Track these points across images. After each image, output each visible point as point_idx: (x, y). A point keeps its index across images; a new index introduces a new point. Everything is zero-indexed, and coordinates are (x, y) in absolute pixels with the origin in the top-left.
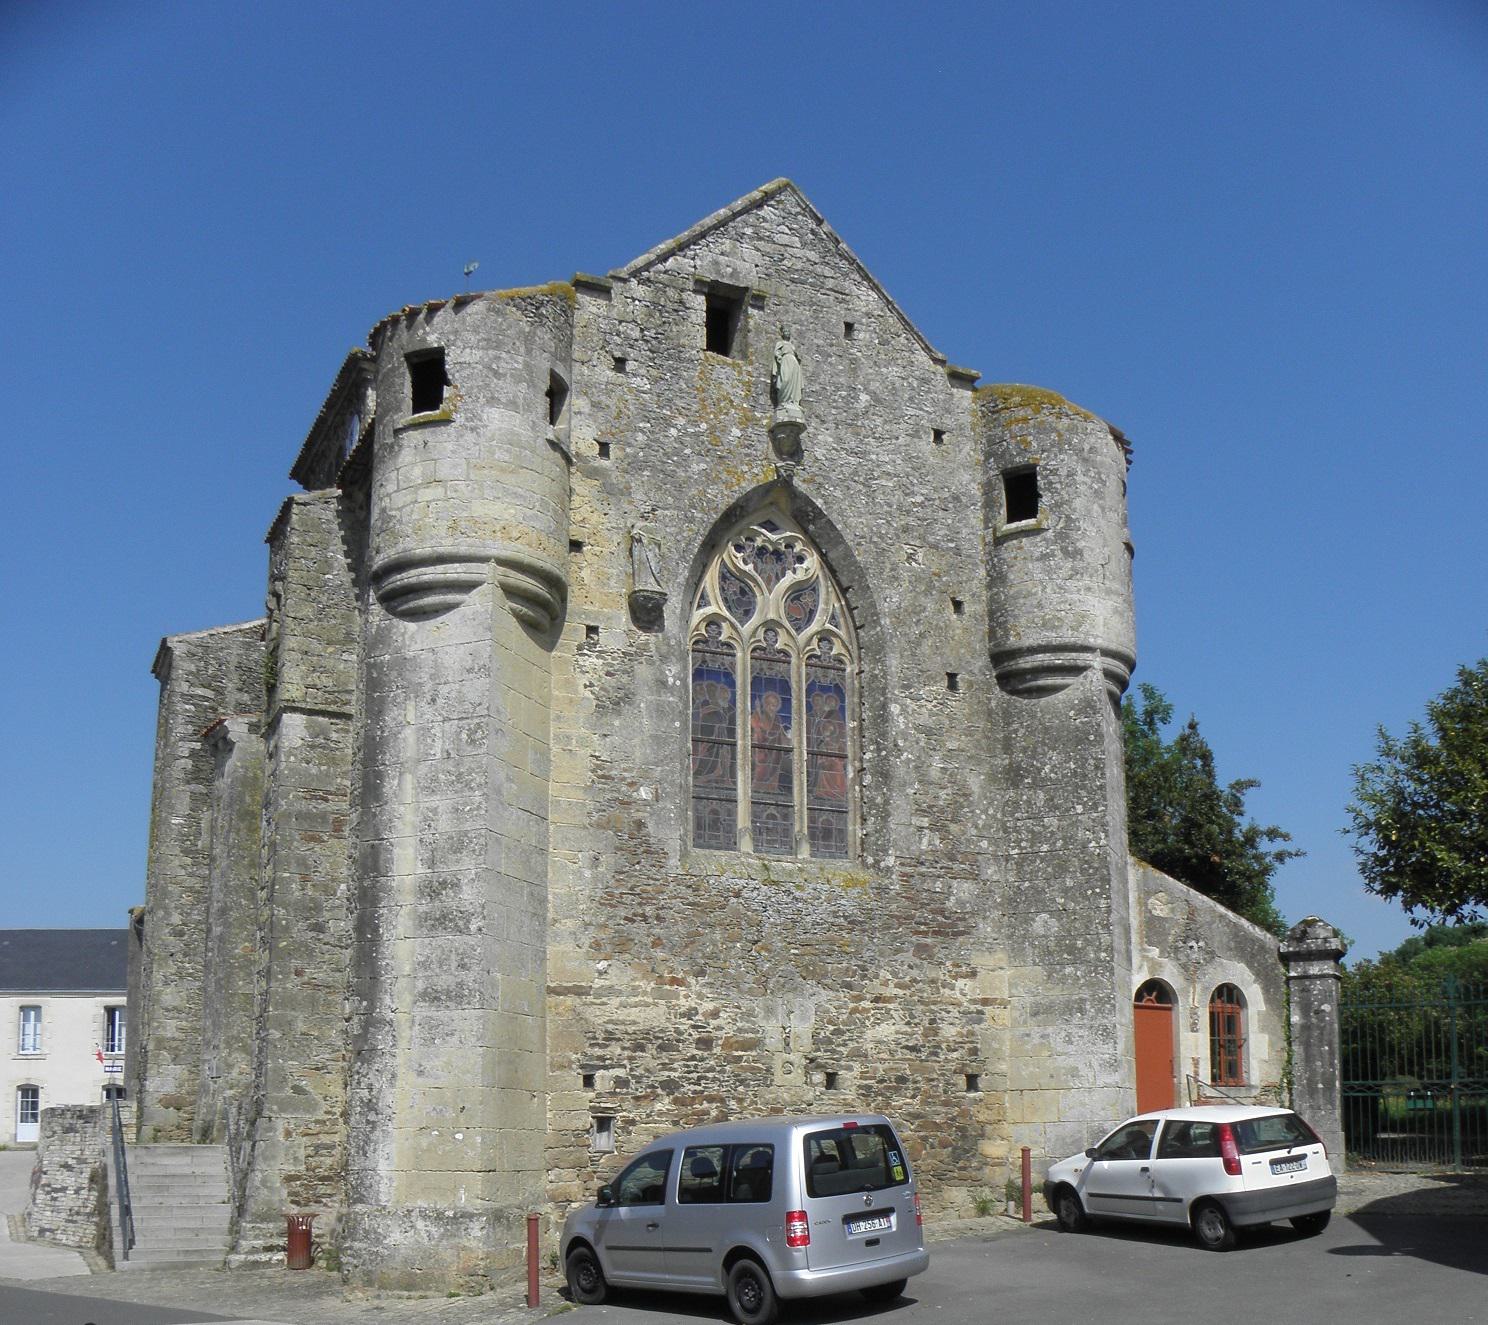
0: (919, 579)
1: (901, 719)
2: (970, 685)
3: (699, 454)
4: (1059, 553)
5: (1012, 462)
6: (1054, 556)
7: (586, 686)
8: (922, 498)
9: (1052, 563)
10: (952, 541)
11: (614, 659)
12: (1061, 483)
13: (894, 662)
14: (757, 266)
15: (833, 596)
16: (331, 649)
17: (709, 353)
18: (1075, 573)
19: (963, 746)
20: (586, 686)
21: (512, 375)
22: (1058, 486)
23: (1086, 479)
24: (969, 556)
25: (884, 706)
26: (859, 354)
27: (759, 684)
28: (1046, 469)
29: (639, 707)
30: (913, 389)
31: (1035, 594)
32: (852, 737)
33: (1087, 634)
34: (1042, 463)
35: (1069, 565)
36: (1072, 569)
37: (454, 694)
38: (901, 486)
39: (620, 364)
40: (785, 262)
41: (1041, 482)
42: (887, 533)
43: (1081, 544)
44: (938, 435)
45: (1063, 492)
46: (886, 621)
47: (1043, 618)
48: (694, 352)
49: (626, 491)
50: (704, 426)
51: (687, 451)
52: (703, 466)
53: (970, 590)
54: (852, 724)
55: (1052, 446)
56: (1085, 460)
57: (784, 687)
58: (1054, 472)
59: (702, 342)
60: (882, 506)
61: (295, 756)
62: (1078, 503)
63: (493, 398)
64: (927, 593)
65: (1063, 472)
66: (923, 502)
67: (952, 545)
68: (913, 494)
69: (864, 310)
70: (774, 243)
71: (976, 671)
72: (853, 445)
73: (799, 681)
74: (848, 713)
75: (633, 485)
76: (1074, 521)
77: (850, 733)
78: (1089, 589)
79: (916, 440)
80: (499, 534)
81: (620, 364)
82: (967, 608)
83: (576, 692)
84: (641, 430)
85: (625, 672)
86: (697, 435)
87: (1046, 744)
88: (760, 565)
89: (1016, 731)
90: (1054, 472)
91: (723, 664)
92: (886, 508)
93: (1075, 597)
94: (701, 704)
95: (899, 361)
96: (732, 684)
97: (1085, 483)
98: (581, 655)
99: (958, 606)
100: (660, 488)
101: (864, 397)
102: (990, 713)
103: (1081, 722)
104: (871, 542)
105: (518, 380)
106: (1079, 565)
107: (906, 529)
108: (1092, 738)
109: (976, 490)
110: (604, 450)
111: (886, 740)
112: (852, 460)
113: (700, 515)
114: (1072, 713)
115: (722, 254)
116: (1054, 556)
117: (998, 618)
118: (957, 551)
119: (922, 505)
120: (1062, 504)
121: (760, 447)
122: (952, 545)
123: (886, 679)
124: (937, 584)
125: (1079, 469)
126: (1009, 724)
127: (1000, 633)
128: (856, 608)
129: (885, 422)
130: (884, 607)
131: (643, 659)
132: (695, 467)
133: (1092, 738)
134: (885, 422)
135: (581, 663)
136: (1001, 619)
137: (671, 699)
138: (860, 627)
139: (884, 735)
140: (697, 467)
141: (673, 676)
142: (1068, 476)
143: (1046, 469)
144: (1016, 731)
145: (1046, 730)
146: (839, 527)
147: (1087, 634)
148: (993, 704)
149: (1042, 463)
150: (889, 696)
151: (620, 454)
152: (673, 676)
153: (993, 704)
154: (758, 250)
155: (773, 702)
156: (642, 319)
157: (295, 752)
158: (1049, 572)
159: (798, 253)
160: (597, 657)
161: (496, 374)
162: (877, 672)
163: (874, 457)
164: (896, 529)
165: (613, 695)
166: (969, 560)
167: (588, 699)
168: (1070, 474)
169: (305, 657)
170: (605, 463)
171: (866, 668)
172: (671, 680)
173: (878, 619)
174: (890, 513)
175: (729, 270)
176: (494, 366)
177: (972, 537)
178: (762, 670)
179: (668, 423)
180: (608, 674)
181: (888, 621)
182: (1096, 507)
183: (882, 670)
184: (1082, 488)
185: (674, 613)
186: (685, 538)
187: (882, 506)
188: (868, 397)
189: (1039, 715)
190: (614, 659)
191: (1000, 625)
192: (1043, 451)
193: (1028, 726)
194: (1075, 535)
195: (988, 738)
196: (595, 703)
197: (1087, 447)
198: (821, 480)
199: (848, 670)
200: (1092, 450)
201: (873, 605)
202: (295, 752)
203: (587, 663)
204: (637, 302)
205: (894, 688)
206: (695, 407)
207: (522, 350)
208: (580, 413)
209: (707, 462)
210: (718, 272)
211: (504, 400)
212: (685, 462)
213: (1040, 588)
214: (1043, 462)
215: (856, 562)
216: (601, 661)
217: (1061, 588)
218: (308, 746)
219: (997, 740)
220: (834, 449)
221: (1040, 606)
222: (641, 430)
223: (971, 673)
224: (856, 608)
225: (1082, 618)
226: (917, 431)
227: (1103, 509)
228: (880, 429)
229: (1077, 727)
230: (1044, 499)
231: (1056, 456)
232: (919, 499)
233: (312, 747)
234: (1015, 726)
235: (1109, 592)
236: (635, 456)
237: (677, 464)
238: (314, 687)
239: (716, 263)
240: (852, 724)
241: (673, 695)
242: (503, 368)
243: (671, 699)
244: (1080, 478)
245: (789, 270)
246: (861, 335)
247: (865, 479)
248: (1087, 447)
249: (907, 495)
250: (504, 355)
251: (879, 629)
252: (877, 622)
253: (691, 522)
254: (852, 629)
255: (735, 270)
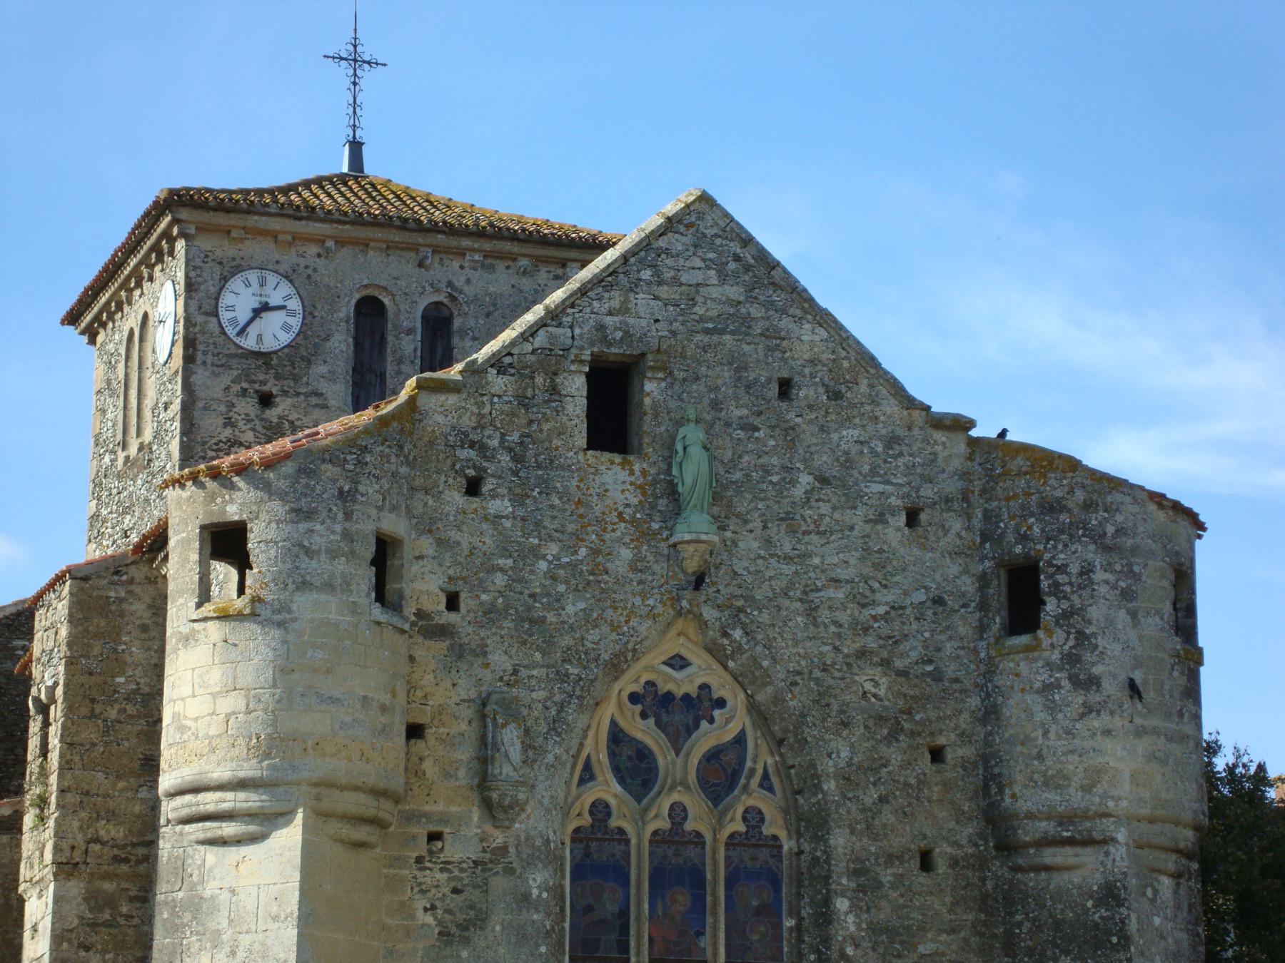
0: (880, 719)
1: (851, 918)
2: (954, 863)
3: (576, 590)
4: (1066, 683)
5: (1010, 552)
6: (1059, 687)
7: (426, 910)
8: (887, 608)
9: (1057, 697)
10: (930, 662)
11: (462, 870)
12: (1070, 584)
13: (841, 841)
14: (657, 321)
15: (764, 749)
16: (121, 784)
17: (590, 452)
18: (1089, 710)
19: (942, 948)
20: (426, 910)
21: (327, 551)
22: (1067, 589)
23: (1109, 576)
24: (956, 680)
25: (827, 901)
26: (799, 420)
27: (661, 878)
28: (1052, 565)
29: (493, 930)
30: (877, 455)
31: (1035, 739)
32: (789, 941)
33: (1104, 796)
34: (1047, 556)
35: (1080, 700)
36: (1084, 704)
37: (257, 947)
38: (852, 597)
39: (473, 488)
40: (697, 309)
41: (1045, 584)
42: (834, 663)
43: (1098, 670)
44: (912, 518)
45: (1075, 598)
46: (830, 786)
47: (1044, 774)
48: (571, 454)
49: (482, 651)
50: (583, 552)
51: (562, 588)
52: (582, 605)
53: (957, 727)
54: (789, 923)
55: (1061, 531)
56: (1107, 549)
57: (696, 880)
58: (1062, 569)
59: (581, 440)
60: (826, 626)
61: (70, 941)
62: (1095, 612)
63: (304, 583)
64: (892, 737)
65: (1074, 569)
66: (887, 613)
67: (929, 668)
68: (874, 603)
69: (807, 356)
70: (681, 284)
71: (964, 842)
72: (787, 548)
73: (715, 871)
74: (785, 906)
75: (489, 641)
76: (1087, 637)
77: (785, 934)
78: (1108, 733)
79: (879, 527)
80: (311, 752)
81: (473, 488)
82: (950, 755)
83: (413, 917)
84: (502, 570)
85: (476, 886)
86: (574, 565)
87: (1057, 946)
88: (665, 718)
89: (1020, 924)
90: (1062, 569)
91: (613, 855)
92: (833, 629)
93: (1088, 744)
94: (582, 911)
95: (857, 420)
96: (625, 882)
97: (1107, 582)
98: (421, 869)
99: (937, 755)
100: (524, 643)
101: (805, 479)
102: (985, 897)
103: (1101, 917)
104: (810, 678)
105: (333, 554)
106: (1094, 698)
107: (862, 654)
108: (1115, 940)
109: (968, 585)
110: (453, 602)
111: (828, 948)
112: (788, 570)
113: (576, 671)
114: (1090, 904)
115: (610, 313)
116: (1059, 687)
117: (992, 767)
118: (937, 676)
119: (885, 617)
120: (1072, 614)
121: (656, 568)
122: (929, 668)
123: (830, 865)
124: (906, 725)
125: (1098, 561)
126: (1011, 914)
127: (994, 790)
128: (793, 767)
129: (834, 508)
130: (828, 766)
131: (500, 868)
132: (570, 609)
133: (1115, 940)
134: (834, 508)
135: (422, 880)
136: (996, 770)
137: (535, 917)
138: (799, 792)
139: (826, 940)
140: (572, 608)
141: (539, 887)
142: (1081, 574)
143: (1052, 565)
144: (1020, 924)
145: (1058, 925)
146: (765, 664)
147: (1104, 796)
148: (989, 885)
149: (1047, 556)
150: (833, 887)
151: (473, 603)
152: (539, 887)
153: (989, 885)
154: (656, 298)
155: (682, 899)
156: (502, 421)
157: (69, 935)
158: (1052, 708)
159: (715, 292)
160: (442, 870)
161: (309, 552)
162: (819, 854)
163: (816, 561)
164: (847, 656)
165: (461, 917)
166: (954, 686)
167: (429, 926)
168: (1087, 571)
169: (86, 799)
170: (452, 617)
171: (806, 847)
172: (535, 892)
173: (820, 782)
174: (839, 635)
175: (619, 334)
176: (306, 543)
177: (961, 652)
178: (665, 857)
179: (536, 553)
180: (456, 891)
181: (833, 784)
182: (1122, 614)
183: (825, 852)
184: (1103, 589)
185: (541, 803)
186: (556, 703)
187: (826, 626)
188: (810, 478)
189: (1049, 903)
190: (462, 870)
191: (994, 777)
192: (1048, 540)
193: (1034, 919)
194: (1088, 657)
195: (981, 934)
196: (437, 931)
197: (1110, 529)
198: (740, 603)
199: (786, 848)
200: (1120, 531)
201: (813, 765)
202: (69, 935)
203: (428, 880)
204: (496, 399)
205: (840, 877)
206: (571, 528)
207: (340, 516)
208: (421, 557)
209: (586, 600)
210: (604, 340)
211: (318, 584)
212: (557, 602)
213: (1040, 732)
214: (1048, 553)
215: (789, 708)
216: (445, 875)
217: (1068, 733)
218: (88, 925)
219: (994, 936)
220: (760, 557)
221: (1040, 757)
222: (502, 570)
223: (956, 844)
224: (793, 767)
225: (1094, 778)
226: (882, 515)
227: (1133, 614)
228: (827, 520)
229: (1096, 925)
230: (1048, 608)
231: (1066, 546)
232: (881, 610)
233: (94, 925)
234: (1019, 917)
235: (1140, 732)
236: (493, 604)
237: (548, 607)
238: (97, 840)
239: (601, 327)
240: (789, 923)
241: (537, 911)
242: (318, 541)
243: (535, 917)
244: (1099, 575)
245: (702, 319)
246: (804, 393)
247: (805, 593)
248: (1110, 529)
249: (863, 606)
250: (318, 527)
251: (820, 796)
252: (817, 788)
253: (563, 681)
254: (789, 793)
255: (626, 332)
